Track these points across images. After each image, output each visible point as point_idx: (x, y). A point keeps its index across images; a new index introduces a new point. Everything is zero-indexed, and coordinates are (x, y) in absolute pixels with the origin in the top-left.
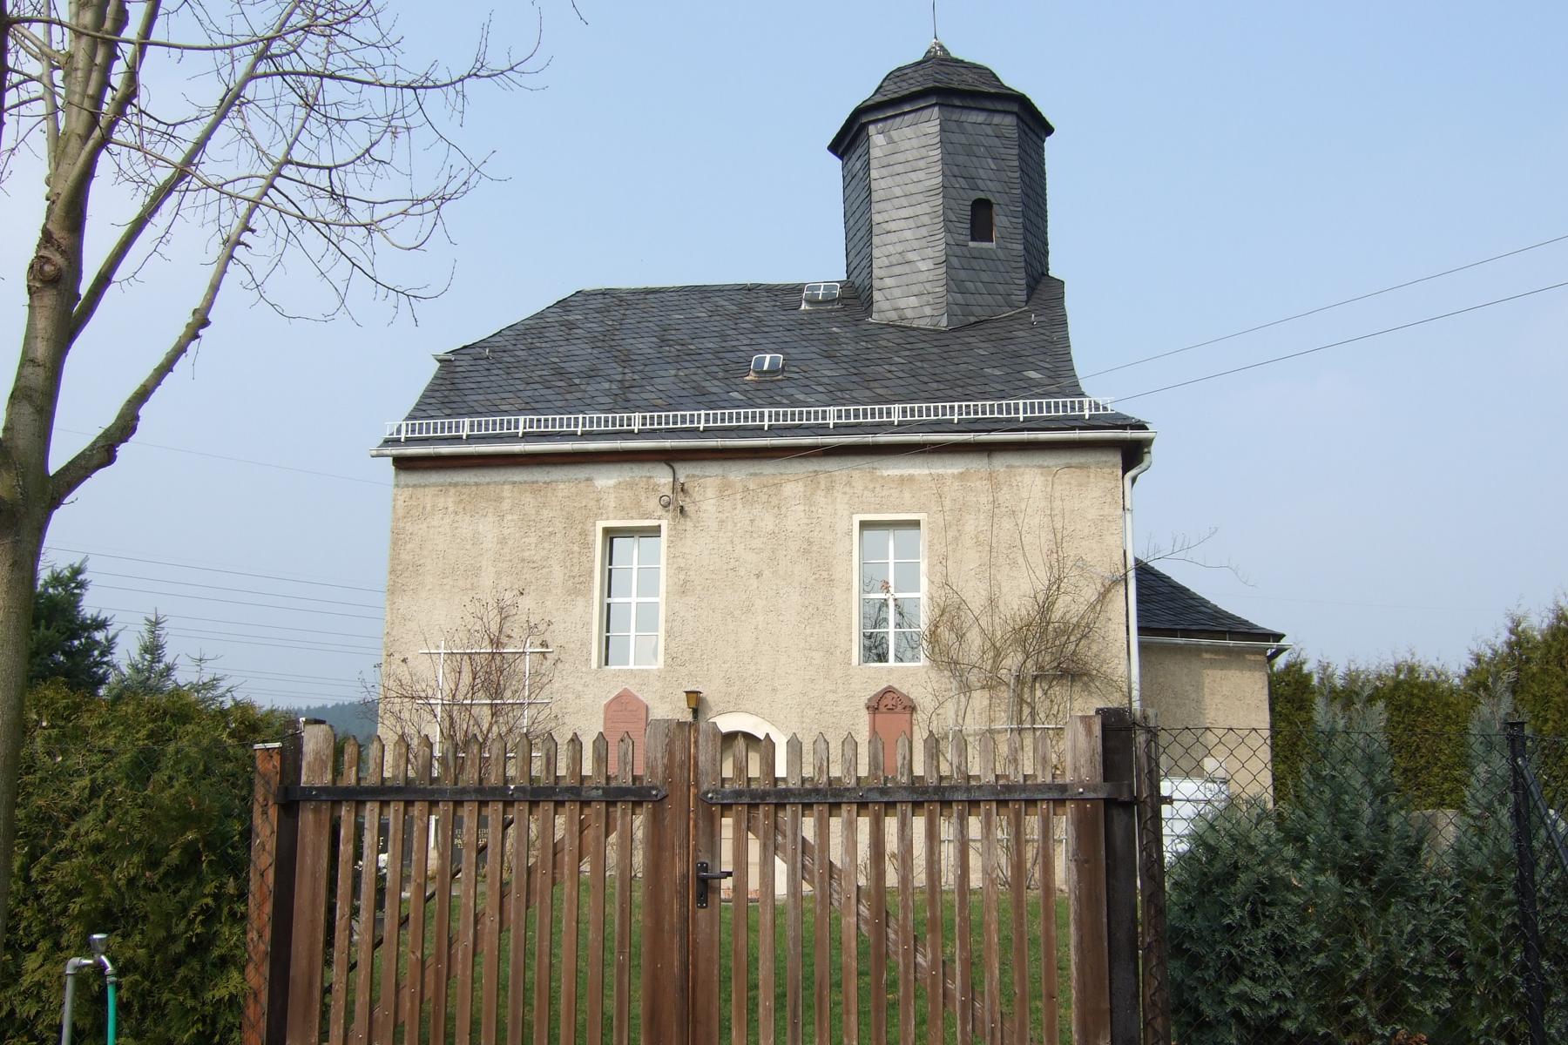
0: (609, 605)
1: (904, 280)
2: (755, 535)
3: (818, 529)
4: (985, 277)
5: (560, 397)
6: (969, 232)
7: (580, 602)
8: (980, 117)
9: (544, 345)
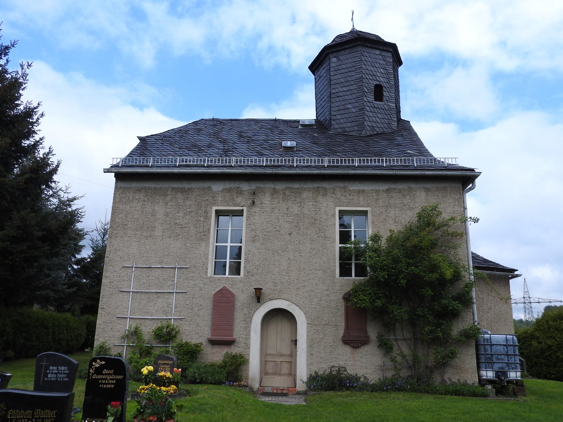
0: (216, 246)
1: (346, 116)
2: (289, 215)
3: (319, 213)
4: (379, 116)
5: (195, 154)
6: (373, 97)
7: (203, 244)
8: (378, 52)
9: (188, 136)
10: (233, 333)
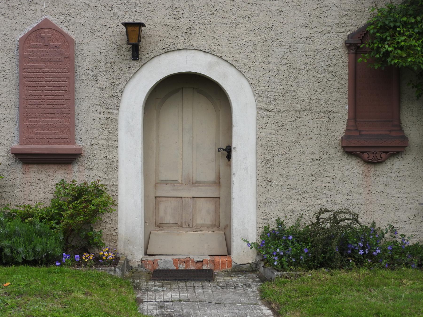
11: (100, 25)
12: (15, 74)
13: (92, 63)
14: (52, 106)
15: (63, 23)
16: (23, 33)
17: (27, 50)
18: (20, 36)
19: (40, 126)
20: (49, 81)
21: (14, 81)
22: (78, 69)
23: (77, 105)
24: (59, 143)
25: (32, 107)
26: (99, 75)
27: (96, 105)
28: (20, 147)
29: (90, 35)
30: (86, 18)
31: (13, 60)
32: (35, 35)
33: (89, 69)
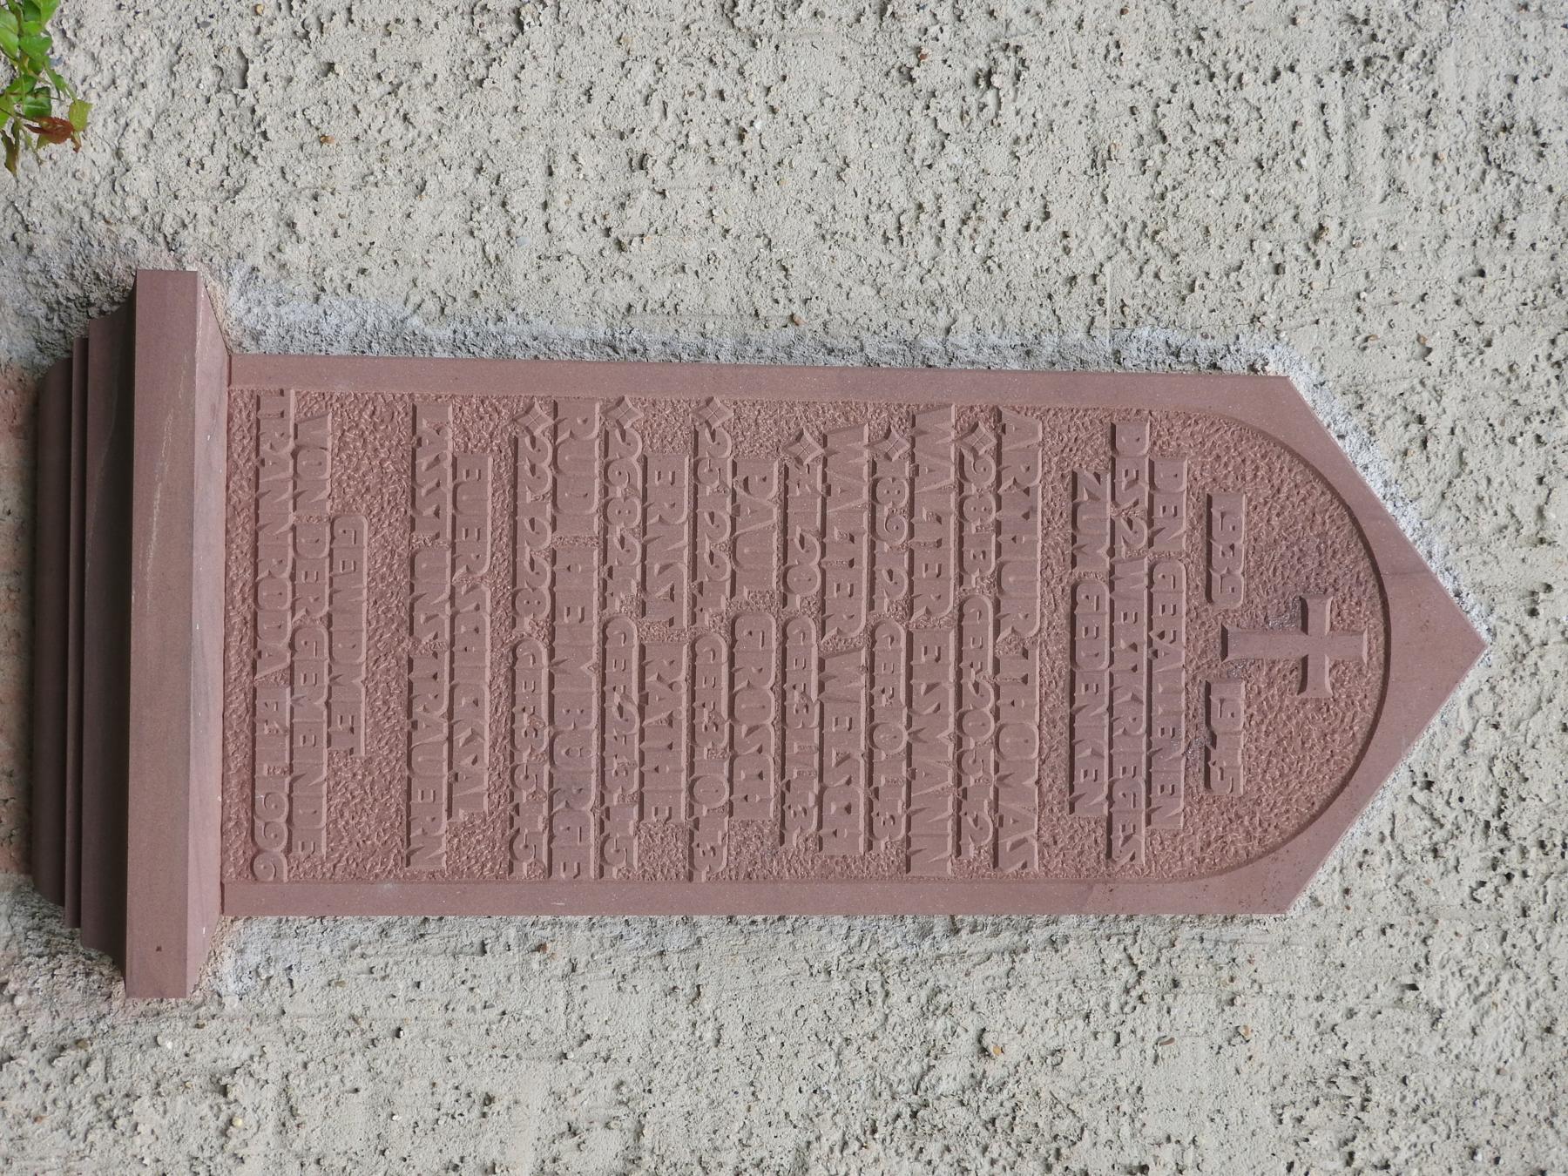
10: (325, 909)
11: (1404, 1154)
12: (942, 320)
13: (1043, 1080)
14: (626, 697)
15: (1421, 797)
16: (1330, 411)
17: (1179, 455)
18: (1301, 383)
19: (422, 565)
20: (880, 671)
21: (875, 305)
22: (992, 944)
23: (636, 939)
24: (238, 760)
25: (618, 492)
26: (933, 1149)
27: (629, 1124)
28: (208, 357)
29: (1315, 1060)
30: (1470, 1015)
31: (1073, 305)
32: (1323, 535)
33: (984, 1051)
